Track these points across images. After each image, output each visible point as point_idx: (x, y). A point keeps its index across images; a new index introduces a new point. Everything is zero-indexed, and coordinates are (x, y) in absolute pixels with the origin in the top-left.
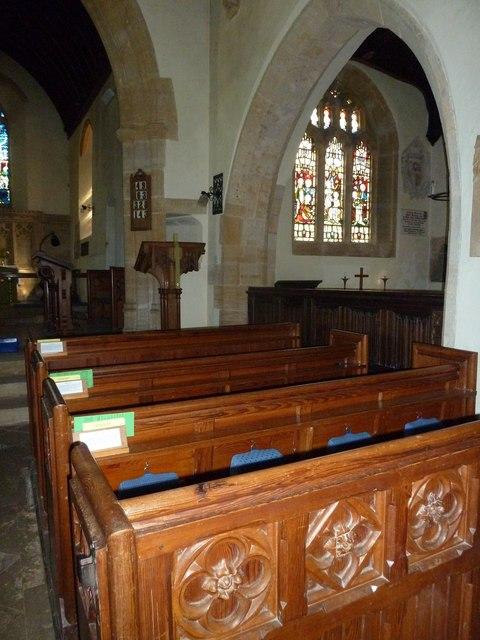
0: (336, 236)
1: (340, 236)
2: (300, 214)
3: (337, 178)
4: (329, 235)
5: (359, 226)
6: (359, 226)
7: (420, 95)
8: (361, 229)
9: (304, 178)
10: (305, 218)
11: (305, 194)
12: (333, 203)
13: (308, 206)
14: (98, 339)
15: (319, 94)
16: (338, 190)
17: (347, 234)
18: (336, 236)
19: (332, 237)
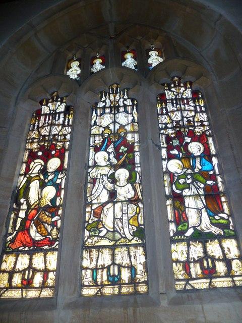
0: (125, 275)
1: (141, 277)
2: (25, 228)
3: (125, 143)
4: (103, 276)
5: (202, 237)
6: (202, 237)
7: (234, 260)
8: (214, 248)
9: (47, 157)
10: (38, 237)
11: (43, 186)
12: (113, 195)
13: (47, 208)
14: (220, 205)
15: (154, 101)
16: (129, 164)
17: (158, 265)
18: (125, 275)
19: (115, 280)
